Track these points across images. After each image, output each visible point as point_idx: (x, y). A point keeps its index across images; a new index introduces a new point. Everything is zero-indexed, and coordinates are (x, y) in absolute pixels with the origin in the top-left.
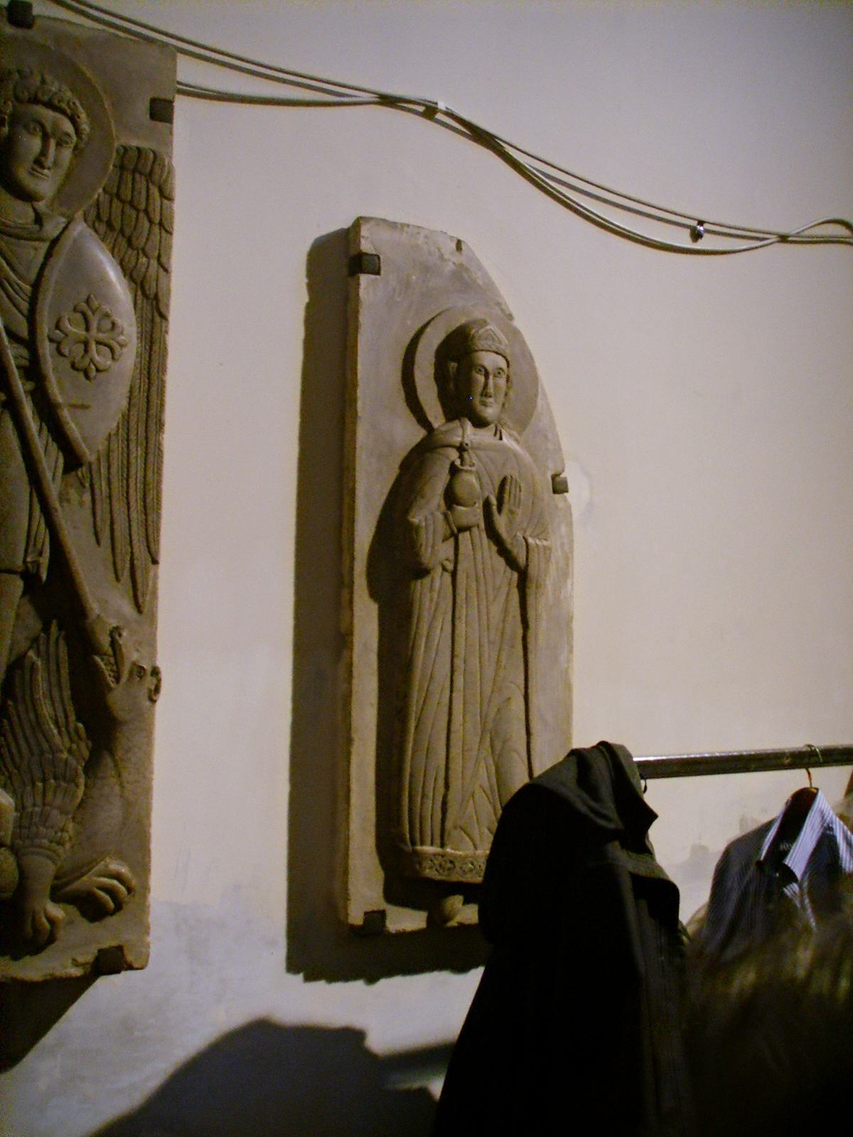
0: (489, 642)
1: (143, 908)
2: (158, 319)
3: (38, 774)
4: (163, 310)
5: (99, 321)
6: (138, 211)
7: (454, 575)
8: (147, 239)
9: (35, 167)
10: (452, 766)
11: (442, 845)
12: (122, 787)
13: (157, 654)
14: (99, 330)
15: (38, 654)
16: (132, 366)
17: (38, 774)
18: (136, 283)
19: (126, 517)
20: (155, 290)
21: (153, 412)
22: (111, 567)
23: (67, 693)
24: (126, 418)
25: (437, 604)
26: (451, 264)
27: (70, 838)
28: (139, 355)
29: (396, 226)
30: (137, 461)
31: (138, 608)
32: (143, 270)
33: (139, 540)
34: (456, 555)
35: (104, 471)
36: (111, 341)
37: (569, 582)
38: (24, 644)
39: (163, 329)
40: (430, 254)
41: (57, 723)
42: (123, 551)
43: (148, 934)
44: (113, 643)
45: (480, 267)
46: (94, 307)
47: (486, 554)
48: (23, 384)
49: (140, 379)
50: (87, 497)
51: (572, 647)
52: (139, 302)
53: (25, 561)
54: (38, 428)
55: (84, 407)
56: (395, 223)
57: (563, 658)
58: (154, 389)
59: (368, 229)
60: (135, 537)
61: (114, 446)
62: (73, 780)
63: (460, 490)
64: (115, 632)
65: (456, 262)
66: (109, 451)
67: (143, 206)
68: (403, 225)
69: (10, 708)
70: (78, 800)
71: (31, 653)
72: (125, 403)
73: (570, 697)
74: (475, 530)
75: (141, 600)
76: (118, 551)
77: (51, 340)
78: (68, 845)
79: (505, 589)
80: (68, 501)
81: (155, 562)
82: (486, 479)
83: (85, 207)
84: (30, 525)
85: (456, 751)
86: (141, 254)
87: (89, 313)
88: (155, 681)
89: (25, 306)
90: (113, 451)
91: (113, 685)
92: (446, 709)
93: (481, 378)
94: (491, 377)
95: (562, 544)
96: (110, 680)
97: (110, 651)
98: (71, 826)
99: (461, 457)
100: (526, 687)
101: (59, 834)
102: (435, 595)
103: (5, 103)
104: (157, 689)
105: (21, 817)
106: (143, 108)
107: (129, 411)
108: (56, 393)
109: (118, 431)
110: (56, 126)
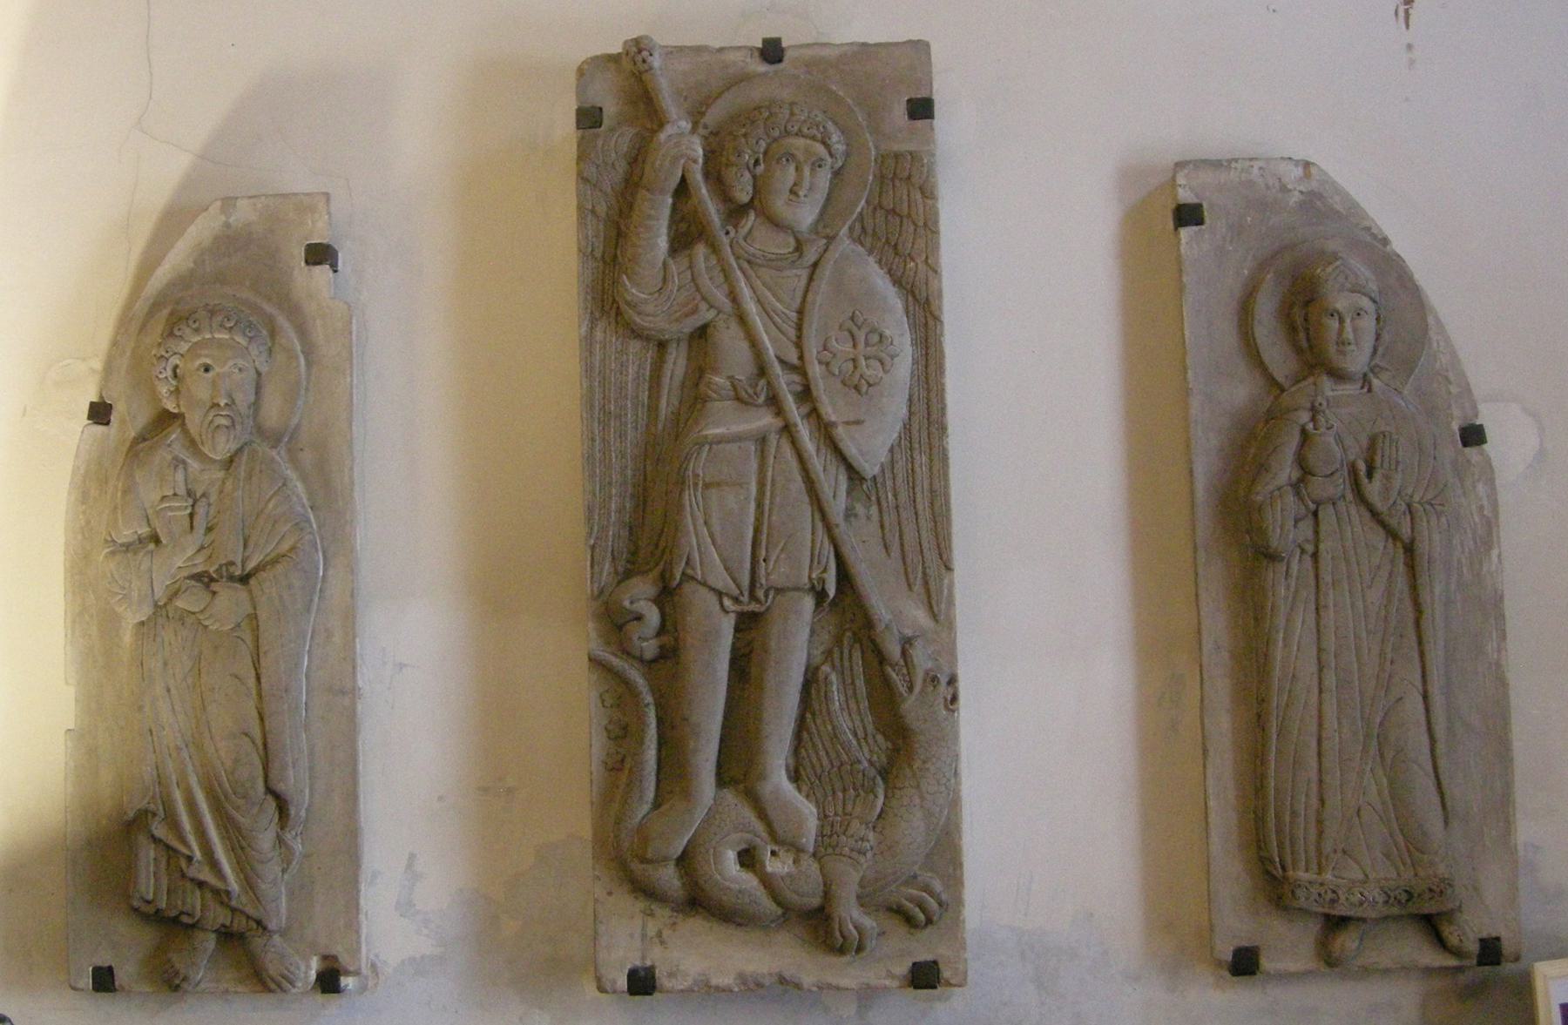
0: (1368, 632)
1: (957, 923)
2: (931, 323)
3: (838, 785)
4: (936, 313)
5: (866, 336)
6: (901, 217)
7: (1315, 556)
8: (913, 244)
9: (791, 197)
10: (1327, 779)
11: (1320, 870)
12: (922, 798)
13: (957, 662)
14: (867, 344)
15: (833, 667)
16: (908, 375)
17: (838, 785)
18: (906, 289)
19: (915, 526)
20: (925, 295)
21: (934, 416)
22: (903, 577)
23: (865, 704)
24: (907, 427)
25: (1296, 591)
26: (1296, 193)
27: (872, 848)
28: (915, 362)
29: (1222, 165)
30: (922, 470)
31: (935, 617)
32: (912, 274)
33: (930, 548)
34: (1316, 533)
35: (889, 483)
36: (881, 353)
37: (1495, 553)
38: (818, 659)
39: (938, 332)
40: (1268, 187)
41: (855, 735)
42: (915, 561)
43: (965, 949)
44: (904, 653)
45: (1338, 190)
46: (859, 324)
47: (1358, 529)
48: (798, 408)
49: (919, 385)
50: (874, 510)
52: (911, 308)
53: (810, 578)
54: (816, 448)
55: (858, 422)
56: (1220, 161)
57: (1490, 647)
58: (933, 395)
60: (925, 545)
61: (898, 456)
62: (872, 791)
63: (1313, 459)
64: (907, 643)
65: (1304, 190)
66: (893, 462)
67: (905, 212)
68: (1230, 161)
69: (808, 720)
70: (878, 810)
71: (826, 668)
72: (905, 411)
74: (1341, 505)
75: (935, 609)
76: (909, 561)
77: (820, 363)
78: (869, 855)
80: (856, 516)
81: (949, 569)
82: (1349, 441)
83: (849, 223)
84: (813, 541)
86: (908, 260)
87: (855, 329)
88: (951, 690)
89: (792, 333)
90: (897, 462)
91: (905, 695)
92: (1314, 712)
93: (1334, 324)
94: (1348, 321)
95: (1481, 508)
96: (903, 690)
97: (902, 662)
98: (871, 835)
99: (1313, 419)
101: (860, 843)
103: (757, 143)
104: (954, 699)
105: (822, 826)
106: (899, 111)
107: (910, 419)
108: (828, 411)
109: (900, 442)
110: (807, 151)
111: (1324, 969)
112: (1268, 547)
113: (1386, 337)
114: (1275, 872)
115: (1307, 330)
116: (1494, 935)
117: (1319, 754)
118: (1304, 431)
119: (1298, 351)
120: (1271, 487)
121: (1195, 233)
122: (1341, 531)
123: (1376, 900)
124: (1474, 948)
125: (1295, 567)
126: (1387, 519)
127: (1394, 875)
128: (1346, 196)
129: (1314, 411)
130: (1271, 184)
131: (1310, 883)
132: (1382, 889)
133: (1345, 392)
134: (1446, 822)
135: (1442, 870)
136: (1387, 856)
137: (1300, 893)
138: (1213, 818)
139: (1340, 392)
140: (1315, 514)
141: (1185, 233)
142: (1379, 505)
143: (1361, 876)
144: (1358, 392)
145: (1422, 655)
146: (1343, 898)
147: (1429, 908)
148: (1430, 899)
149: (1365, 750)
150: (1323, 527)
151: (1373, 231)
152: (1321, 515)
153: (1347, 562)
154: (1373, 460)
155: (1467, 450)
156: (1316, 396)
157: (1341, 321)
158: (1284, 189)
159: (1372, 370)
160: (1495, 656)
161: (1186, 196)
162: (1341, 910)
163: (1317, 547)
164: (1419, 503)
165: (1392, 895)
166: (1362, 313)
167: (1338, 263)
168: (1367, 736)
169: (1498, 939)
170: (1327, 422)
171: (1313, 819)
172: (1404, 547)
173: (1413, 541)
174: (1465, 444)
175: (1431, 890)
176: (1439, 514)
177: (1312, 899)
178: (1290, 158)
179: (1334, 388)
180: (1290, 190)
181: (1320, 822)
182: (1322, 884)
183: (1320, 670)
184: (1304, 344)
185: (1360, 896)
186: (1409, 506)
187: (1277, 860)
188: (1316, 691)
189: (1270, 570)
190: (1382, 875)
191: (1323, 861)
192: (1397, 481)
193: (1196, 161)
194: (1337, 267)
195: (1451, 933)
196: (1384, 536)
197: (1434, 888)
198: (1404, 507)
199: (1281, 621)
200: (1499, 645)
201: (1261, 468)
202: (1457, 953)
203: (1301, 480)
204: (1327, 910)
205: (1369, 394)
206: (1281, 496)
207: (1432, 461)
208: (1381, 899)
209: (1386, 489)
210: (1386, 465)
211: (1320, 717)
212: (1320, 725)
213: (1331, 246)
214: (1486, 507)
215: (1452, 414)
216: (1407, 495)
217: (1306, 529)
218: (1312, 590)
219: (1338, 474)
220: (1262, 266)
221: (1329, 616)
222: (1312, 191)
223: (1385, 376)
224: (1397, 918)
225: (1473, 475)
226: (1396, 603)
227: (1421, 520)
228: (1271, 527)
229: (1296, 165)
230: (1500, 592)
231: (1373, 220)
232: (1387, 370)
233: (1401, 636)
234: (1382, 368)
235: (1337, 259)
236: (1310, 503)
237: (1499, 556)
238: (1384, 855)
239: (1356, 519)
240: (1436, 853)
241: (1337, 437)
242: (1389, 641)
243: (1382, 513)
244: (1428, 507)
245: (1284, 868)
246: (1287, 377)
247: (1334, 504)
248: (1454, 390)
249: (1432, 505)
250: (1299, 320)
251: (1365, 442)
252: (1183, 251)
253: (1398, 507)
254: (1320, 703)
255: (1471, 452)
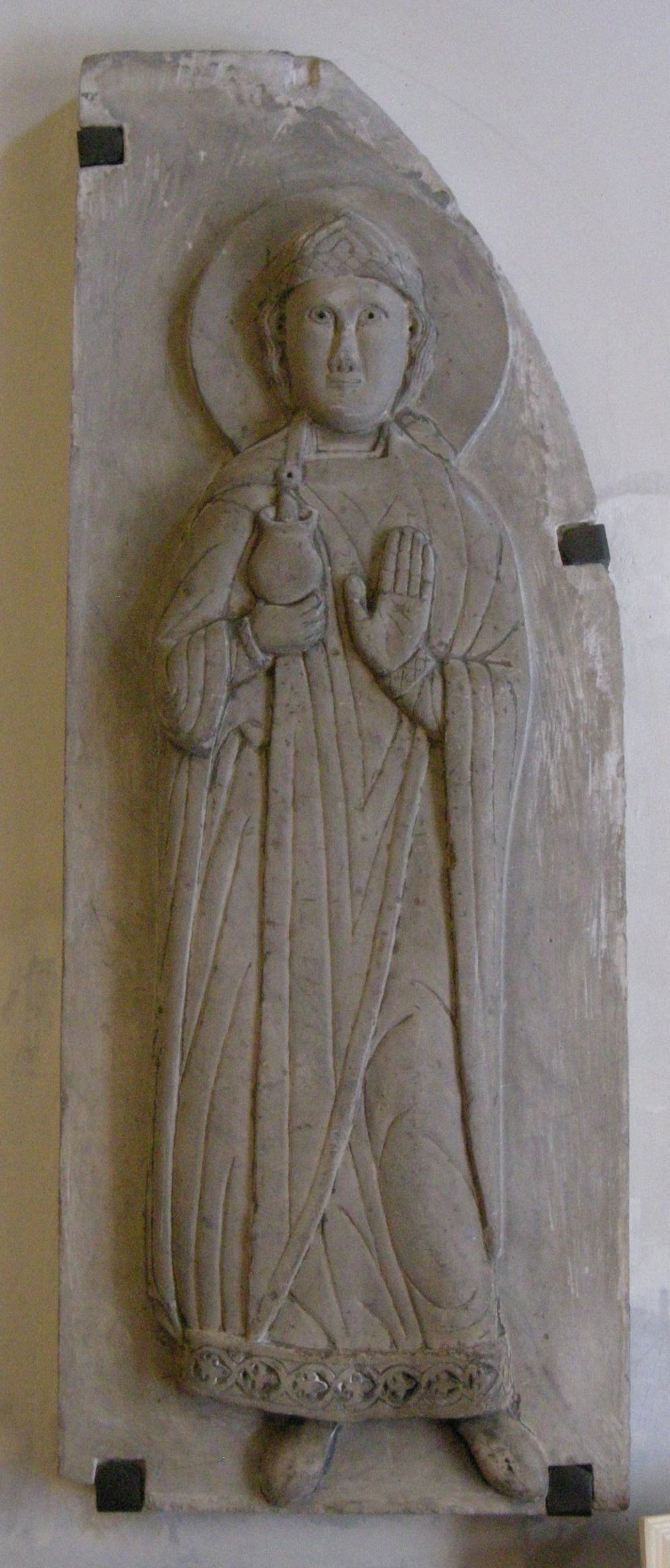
7: (265, 749)
10: (263, 1158)
11: (247, 1330)
25: (228, 813)
26: (291, 111)
34: (270, 707)
37: (611, 759)
40: (240, 99)
45: (366, 106)
47: (346, 702)
51: (622, 902)
56: (160, 54)
59: (97, 79)
63: (266, 570)
68: (176, 55)
73: (620, 1021)
74: (318, 658)
79: (395, 776)
82: (340, 543)
85: (274, 1124)
92: (249, 1037)
94: (351, 326)
95: (592, 674)
99: (277, 502)
100: (455, 993)
102: (223, 797)
111: (258, 1505)
112: (177, 731)
113: (429, 363)
114: (171, 1330)
115: (281, 345)
116: (581, 1460)
117: (254, 1116)
118: (258, 525)
119: (268, 383)
120: (191, 623)
121: (106, 175)
122: (314, 706)
123: (349, 1388)
124: (539, 1483)
125: (228, 773)
126: (396, 684)
127: (386, 1347)
128: (383, 121)
129: (279, 487)
130: (246, 97)
131: (228, 1351)
132: (360, 1367)
133: (341, 455)
134: (489, 1246)
135: (474, 1338)
136: (371, 1306)
137: (212, 1371)
138: (69, 1219)
139: (332, 456)
140: (271, 673)
141: (89, 177)
142: (386, 662)
143: (323, 1344)
144: (365, 455)
145: (452, 938)
146: (287, 1382)
147: (447, 1408)
148: (450, 1391)
149: (338, 1109)
150: (283, 696)
151: (423, 178)
152: (279, 673)
153: (322, 758)
154: (379, 579)
155: (571, 569)
156: (285, 459)
157: (338, 327)
158: (269, 103)
159: (398, 420)
160: (604, 946)
161: (95, 114)
162: (283, 1405)
163: (269, 732)
164: (465, 660)
165: (381, 1381)
166: (375, 313)
167: (339, 224)
168: (343, 1087)
169: (588, 1468)
170: (300, 507)
171: (237, 1227)
172: (430, 739)
173: (444, 724)
174: (567, 561)
175: (451, 1375)
176: (495, 681)
177: (231, 1381)
178: (287, 53)
179: (321, 448)
180: (280, 107)
181: (249, 1238)
182: (249, 1355)
183: (263, 956)
184: (275, 368)
185: (317, 1379)
186: (442, 663)
187: (174, 1305)
188: (253, 998)
189: (184, 775)
190: (361, 1342)
191: (253, 1313)
192: (423, 615)
193: (118, 53)
194: (337, 231)
195: (492, 1456)
196: (395, 715)
197: (458, 1372)
198: (432, 664)
199: (197, 870)
200: (610, 926)
201: (182, 587)
202: (502, 1489)
203: (247, 611)
204: (260, 1404)
205: (384, 460)
206: (205, 638)
207: (493, 582)
208: (358, 1390)
209: (400, 631)
210: (402, 586)
211: (258, 1047)
212: (257, 1062)
213: (343, 199)
214: (599, 674)
215: (546, 506)
216: (441, 643)
217: (252, 700)
218: (257, 813)
219: (313, 601)
220: (217, 234)
221: (284, 866)
222: (319, 108)
223: (421, 432)
224: (394, 1423)
225: (580, 614)
226: (410, 840)
227: (461, 688)
228: (184, 696)
229: (297, 66)
230: (617, 830)
231: (425, 160)
232: (425, 419)
233: (417, 902)
234: (417, 418)
235: (338, 218)
236: (259, 653)
237: (621, 761)
238: (366, 1305)
239: (343, 683)
240: (466, 1307)
241: (318, 534)
242: (391, 908)
243: (389, 675)
244: (475, 665)
245: (184, 1320)
246: (244, 429)
247: (305, 655)
248: (552, 461)
249: (486, 664)
250: (269, 329)
251: (367, 543)
252: (81, 208)
253: (421, 665)
254: (259, 1020)
255: (581, 576)
